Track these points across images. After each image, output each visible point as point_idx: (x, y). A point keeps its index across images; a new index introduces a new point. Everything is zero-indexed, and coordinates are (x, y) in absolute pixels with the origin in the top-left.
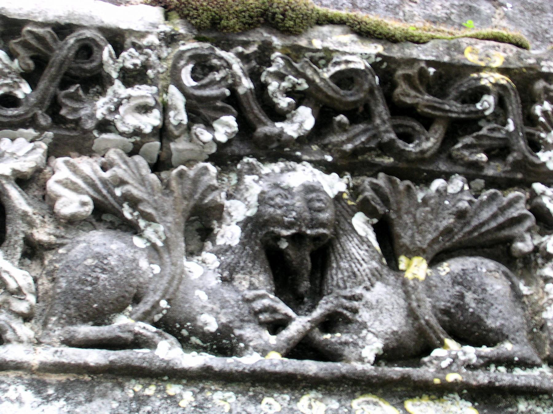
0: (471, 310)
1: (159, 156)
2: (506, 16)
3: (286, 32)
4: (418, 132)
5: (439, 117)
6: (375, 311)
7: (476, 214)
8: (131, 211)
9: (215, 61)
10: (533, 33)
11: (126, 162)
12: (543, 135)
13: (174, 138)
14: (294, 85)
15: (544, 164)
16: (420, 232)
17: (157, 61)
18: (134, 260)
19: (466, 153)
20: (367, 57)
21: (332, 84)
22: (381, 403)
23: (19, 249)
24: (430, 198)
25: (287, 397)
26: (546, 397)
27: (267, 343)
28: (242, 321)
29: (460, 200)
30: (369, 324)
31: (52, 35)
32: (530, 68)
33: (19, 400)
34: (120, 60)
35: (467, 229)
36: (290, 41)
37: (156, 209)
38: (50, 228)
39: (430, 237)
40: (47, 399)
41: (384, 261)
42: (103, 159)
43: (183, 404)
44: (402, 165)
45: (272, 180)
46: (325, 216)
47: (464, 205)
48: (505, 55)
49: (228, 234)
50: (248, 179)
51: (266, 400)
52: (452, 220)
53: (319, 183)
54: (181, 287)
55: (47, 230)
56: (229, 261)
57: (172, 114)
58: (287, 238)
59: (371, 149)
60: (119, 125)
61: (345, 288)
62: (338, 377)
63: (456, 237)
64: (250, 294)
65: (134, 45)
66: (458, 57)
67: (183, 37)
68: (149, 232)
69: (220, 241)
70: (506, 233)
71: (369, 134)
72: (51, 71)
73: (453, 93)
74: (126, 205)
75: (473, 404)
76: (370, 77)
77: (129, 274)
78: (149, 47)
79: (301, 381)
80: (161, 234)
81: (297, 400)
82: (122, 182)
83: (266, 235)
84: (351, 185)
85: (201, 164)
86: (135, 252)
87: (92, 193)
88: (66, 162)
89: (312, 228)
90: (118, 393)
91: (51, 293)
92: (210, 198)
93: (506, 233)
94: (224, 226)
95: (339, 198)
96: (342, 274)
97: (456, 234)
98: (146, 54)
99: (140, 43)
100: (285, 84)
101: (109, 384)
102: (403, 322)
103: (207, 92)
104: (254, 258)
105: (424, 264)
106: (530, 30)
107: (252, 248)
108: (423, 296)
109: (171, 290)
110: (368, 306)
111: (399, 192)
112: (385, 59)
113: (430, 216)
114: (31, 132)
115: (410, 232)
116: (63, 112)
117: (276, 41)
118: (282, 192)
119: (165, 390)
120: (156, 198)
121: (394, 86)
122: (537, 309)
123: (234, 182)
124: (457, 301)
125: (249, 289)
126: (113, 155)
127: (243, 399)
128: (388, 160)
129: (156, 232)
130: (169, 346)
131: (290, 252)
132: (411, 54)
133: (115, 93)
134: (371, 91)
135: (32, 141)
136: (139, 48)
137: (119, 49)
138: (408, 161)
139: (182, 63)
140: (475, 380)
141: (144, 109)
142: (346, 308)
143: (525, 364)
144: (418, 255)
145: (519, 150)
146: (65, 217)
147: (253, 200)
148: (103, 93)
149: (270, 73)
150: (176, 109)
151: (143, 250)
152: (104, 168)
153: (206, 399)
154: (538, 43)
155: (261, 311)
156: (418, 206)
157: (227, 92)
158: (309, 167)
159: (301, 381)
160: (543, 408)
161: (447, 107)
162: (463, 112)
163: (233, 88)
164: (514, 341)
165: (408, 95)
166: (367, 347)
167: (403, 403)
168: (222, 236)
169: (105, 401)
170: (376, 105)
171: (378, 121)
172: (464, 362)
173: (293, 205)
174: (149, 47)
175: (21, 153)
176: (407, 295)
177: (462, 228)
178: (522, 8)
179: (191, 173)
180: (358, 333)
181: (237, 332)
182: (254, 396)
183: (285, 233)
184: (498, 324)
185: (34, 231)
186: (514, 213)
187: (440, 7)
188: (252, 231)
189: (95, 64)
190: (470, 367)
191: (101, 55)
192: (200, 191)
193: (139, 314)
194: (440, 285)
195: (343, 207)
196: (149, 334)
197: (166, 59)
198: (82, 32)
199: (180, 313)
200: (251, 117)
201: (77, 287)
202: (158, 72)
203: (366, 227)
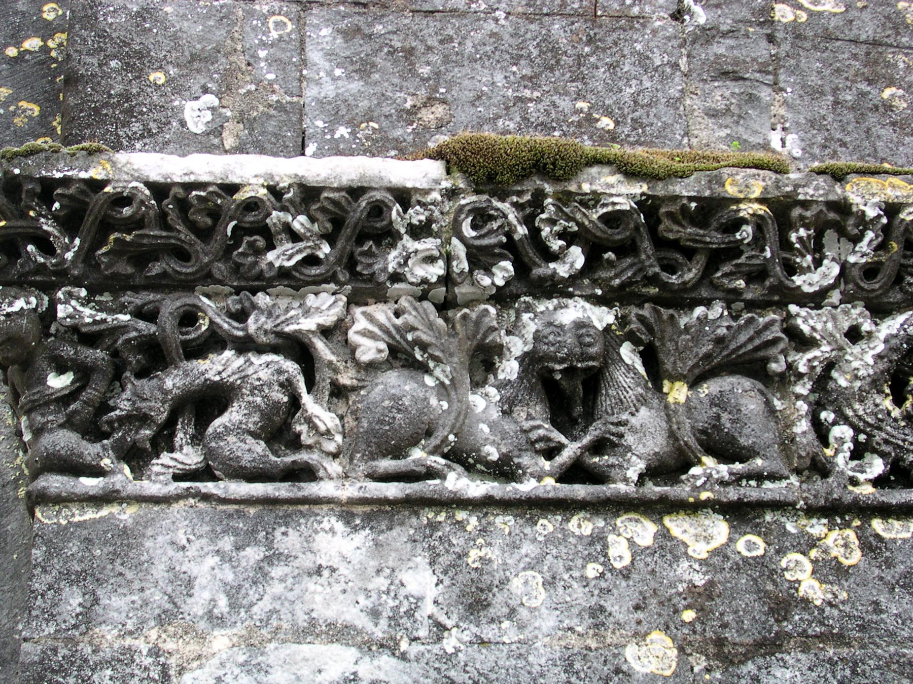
0: (726, 430)
1: (445, 297)
2: (785, 102)
3: (557, 180)
4: (681, 264)
5: (701, 248)
6: (639, 435)
7: (734, 337)
8: (421, 353)
9: (492, 212)
10: (810, 121)
11: (415, 309)
12: (798, 260)
13: (456, 284)
14: (565, 228)
15: (799, 287)
16: (681, 359)
17: (440, 216)
18: (426, 399)
19: (725, 281)
20: (633, 197)
21: (600, 225)
22: (642, 519)
23: (327, 393)
24: (691, 327)
25: (559, 518)
26: (790, 508)
27: (542, 469)
28: (520, 450)
29: (719, 327)
30: (633, 447)
31: (346, 199)
32: (787, 196)
33: (332, 531)
34: (407, 216)
35: (725, 353)
36: (559, 188)
37: (443, 351)
38: (352, 373)
39: (690, 363)
40: (355, 529)
41: (650, 385)
42: (396, 306)
43: (469, 528)
44: (666, 295)
45: (547, 319)
46: (593, 350)
47: (722, 331)
48: (764, 184)
49: (508, 370)
50: (526, 317)
51: (541, 521)
52: (711, 347)
53: (589, 318)
54: (467, 421)
55: (350, 375)
56: (508, 395)
57: (454, 263)
58: (561, 371)
59: (637, 282)
60: (408, 276)
61: (613, 414)
62: (603, 500)
63: (715, 361)
64: (527, 425)
65: (419, 203)
66: (718, 190)
67: (463, 191)
68: (438, 372)
69: (501, 376)
70: (762, 354)
71: (635, 268)
72: (347, 232)
73: (715, 225)
74: (416, 348)
75: (724, 517)
76: (635, 216)
77: (421, 413)
78: (432, 204)
79: (572, 504)
80: (448, 373)
81: (568, 520)
82: (413, 329)
83: (541, 369)
84: (619, 315)
85: (483, 307)
86: (426, 391)
87: (387, 339)
88: (364, 313)
89: (583, 361)
90: (414, 520)
91: (355, 430)
92: (491, 338)
93: (762, 354)
94: (504, 361)
95: (608, 329)
96: (610, 400)
97: (715, 358)
98: (430, 210)
99: (424, 200)
100: (556, 228)
101: (407, 513)
102: (665, 443)
103: (486, 242)
104: (531, 390)
105: (685, 388)
106: (808, 118)
107: (529, 381)
108: (683, 418)
109: (458, 425)
110: (633, 430)
111: (664, 322)
112: (649, 197)
113: (690, 344)
114: (332, 286)
115: (672, 359)
116: (359, 268)
117: (548, 188)
118: (555, 329)
119: (454, 515)
120: (443, 341)
121: (659, 222)
122: (789, 423)
123: (513, 319)
124: (714, 422)
125: (527, 419)
126: (404, 302)
127: (521, 521)
128: (654, 291)
129: (444, 371)
130: (457, 476)
131: (564, 383)
132: (674, 191)
133: (404, 247)
134: (637, 228)
135: (333, 294)
136: (423, 205)
137: (406, 206)
138: (672, 291)
139: (463, 216)
140: (725, 497)
141: (430, 260)
142: (613, 434)
143: (774, 477)
144: (680, 380)
145: (775, 276)
146: (364, 363)
147: (530, 337)
148: (393, 245)
149: (542, 220)
150: (458, 258)
151: (433, 388)
152: (397, 314)
153: (489, 523)
154: (815, 132)
155: (537, 441)
156: (681, 333)
157: (504, 239)
158: (582, 302)
159: (572, 504)
160: (787, 517)
161: (708, 239)
162: (723, 243)
163: (509, 235)
164: (765, 457)
165: (671, 231)
166: (631, 469)
167: (662, 518)
168: (503, 371)
169: (403, 528)
170: (642, 242)
171: (643, 257)
172: (717, 480)
173: (565, 342)
174: (432, 204)
175: (324, 307)
176: (669, 419)
177: (721, 352)
178: (802, 92)
179: (474, 316)
180: (623, 455)
181: (516, 460)
182: (531, 518)
183: (558, 367)
184: (750, 442)
185: (339, 376)
186: (769, 336)
187: (720, 98)
188: (529, 365)
189: (385, 223)
190: (722, 483)
191: (390, 215)
192: (482, 332)
193: (430, 448)
194: (698, 407)
195: (612, 338)
196: (439, 467)
197: (448, 213)
198: (372, 193)
199: (466, 444)
200: (526, 260)
201: (377, 427)
202: (442, 226)
203: (632, 355)
